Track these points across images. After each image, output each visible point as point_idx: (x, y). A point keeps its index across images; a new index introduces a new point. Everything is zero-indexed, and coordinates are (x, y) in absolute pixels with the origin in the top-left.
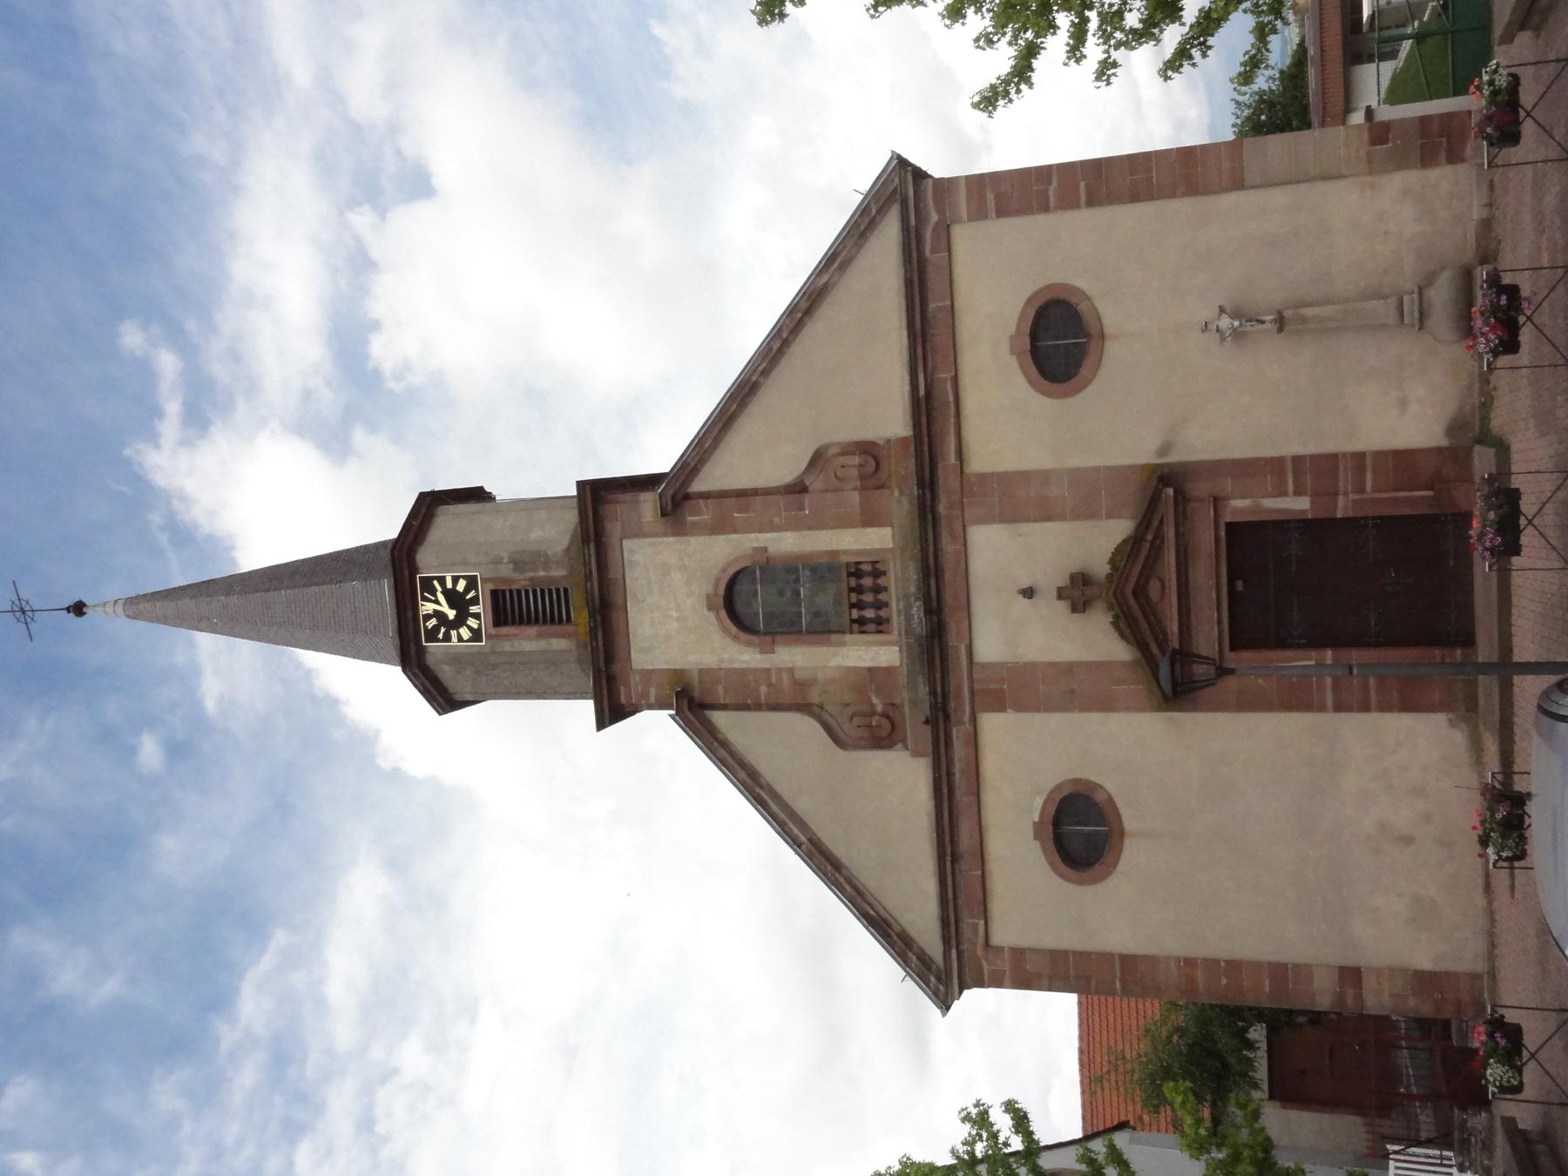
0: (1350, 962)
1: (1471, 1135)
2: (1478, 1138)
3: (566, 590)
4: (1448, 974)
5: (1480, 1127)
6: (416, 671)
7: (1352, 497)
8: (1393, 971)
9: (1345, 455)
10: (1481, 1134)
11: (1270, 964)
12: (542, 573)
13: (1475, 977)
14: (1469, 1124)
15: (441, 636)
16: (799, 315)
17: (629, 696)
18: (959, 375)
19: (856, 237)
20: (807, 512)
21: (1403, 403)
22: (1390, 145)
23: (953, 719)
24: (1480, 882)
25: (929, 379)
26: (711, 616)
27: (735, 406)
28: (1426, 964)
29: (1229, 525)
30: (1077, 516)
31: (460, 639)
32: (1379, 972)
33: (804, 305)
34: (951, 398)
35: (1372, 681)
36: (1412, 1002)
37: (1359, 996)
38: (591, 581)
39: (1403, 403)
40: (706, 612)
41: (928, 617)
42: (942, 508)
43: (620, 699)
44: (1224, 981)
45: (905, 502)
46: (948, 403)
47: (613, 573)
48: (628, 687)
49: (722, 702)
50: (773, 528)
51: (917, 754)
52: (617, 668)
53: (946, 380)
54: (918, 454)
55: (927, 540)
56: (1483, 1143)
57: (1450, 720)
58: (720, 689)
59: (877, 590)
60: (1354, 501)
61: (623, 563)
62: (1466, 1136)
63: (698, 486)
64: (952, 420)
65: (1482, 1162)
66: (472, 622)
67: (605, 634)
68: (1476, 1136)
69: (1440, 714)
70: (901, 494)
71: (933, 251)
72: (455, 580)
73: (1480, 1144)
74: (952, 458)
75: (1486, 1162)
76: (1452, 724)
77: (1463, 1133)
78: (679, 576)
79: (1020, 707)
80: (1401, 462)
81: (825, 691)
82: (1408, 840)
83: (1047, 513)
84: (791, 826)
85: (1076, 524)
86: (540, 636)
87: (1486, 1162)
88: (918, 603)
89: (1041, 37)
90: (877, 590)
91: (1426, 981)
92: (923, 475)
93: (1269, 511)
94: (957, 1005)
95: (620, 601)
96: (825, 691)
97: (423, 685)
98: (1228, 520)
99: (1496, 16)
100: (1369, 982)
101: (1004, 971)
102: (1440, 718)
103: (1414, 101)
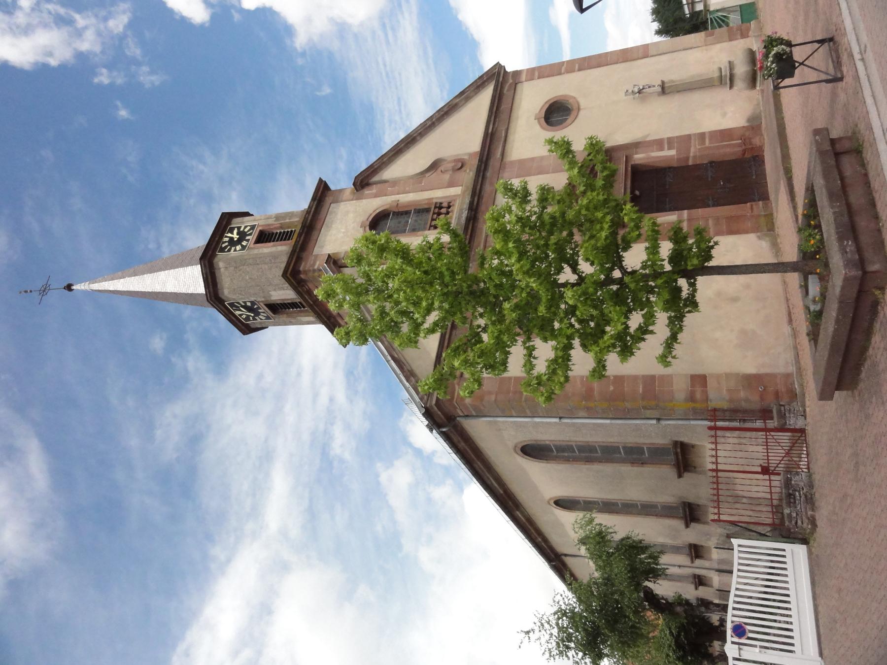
0: (700, 371)
1: (796, 490)
2: (802, 493)
4: (767, 375)
5: (802, 484)
6: (206, 262)
7: (698, 147)
8: (728, 376)
9: (695, 134)
10: (803, 489)
11: (643, 376)
12: (287, 221)
13: (788, 376)
14: (793, 482)
16: (443, 113)
17: (305, 267)
18: (509, 128)
19: (475, 87)
23: (471, 259)
24: (785, 319)
25: (494, 129)
27: (403, 145)
28: (751, 369)
31: (261, 319)
32: (718, 377)
33: (445, 109)
34: (503, 135)
36: (742, 394)
37: (705, 393)
38: (309, 215)
40: (359, 228)
41: (470, 211)
42: (488, 174)
43: (299, 267)
44: (612, 388)
46: (524, 523)
47: (322, 215)
48: (306, 264)
52: (304, 255)
54: (480, 160)
55: (478, 182)
56: (806, 496)
60: (699, 149)
61: (328, 212)
62: (791, 491)
63: (376, 178)
64: (502, 142)
65: (806, 513)
66: (244, 243)
67: (305, 238)
68: (799, 492)
69: (752, 234)
71: (508, 90)
73: (803, 497)
74: (498, 155)
75: (810, 513)
76: (759, 238)
77: (789, 490)
78: (352, 215)
80: (725, 134)
82: (735, 300)
85: (553, 175)
86: (274, 246)
87: (810, 513)
89: (646, 313)
90: (448, 213)
91: (752, 381)
92: (483, 157)
93: (653, 157)
95: (319, 227)
97: (206, 274)
100: (711, 384)
102: (752, 237)
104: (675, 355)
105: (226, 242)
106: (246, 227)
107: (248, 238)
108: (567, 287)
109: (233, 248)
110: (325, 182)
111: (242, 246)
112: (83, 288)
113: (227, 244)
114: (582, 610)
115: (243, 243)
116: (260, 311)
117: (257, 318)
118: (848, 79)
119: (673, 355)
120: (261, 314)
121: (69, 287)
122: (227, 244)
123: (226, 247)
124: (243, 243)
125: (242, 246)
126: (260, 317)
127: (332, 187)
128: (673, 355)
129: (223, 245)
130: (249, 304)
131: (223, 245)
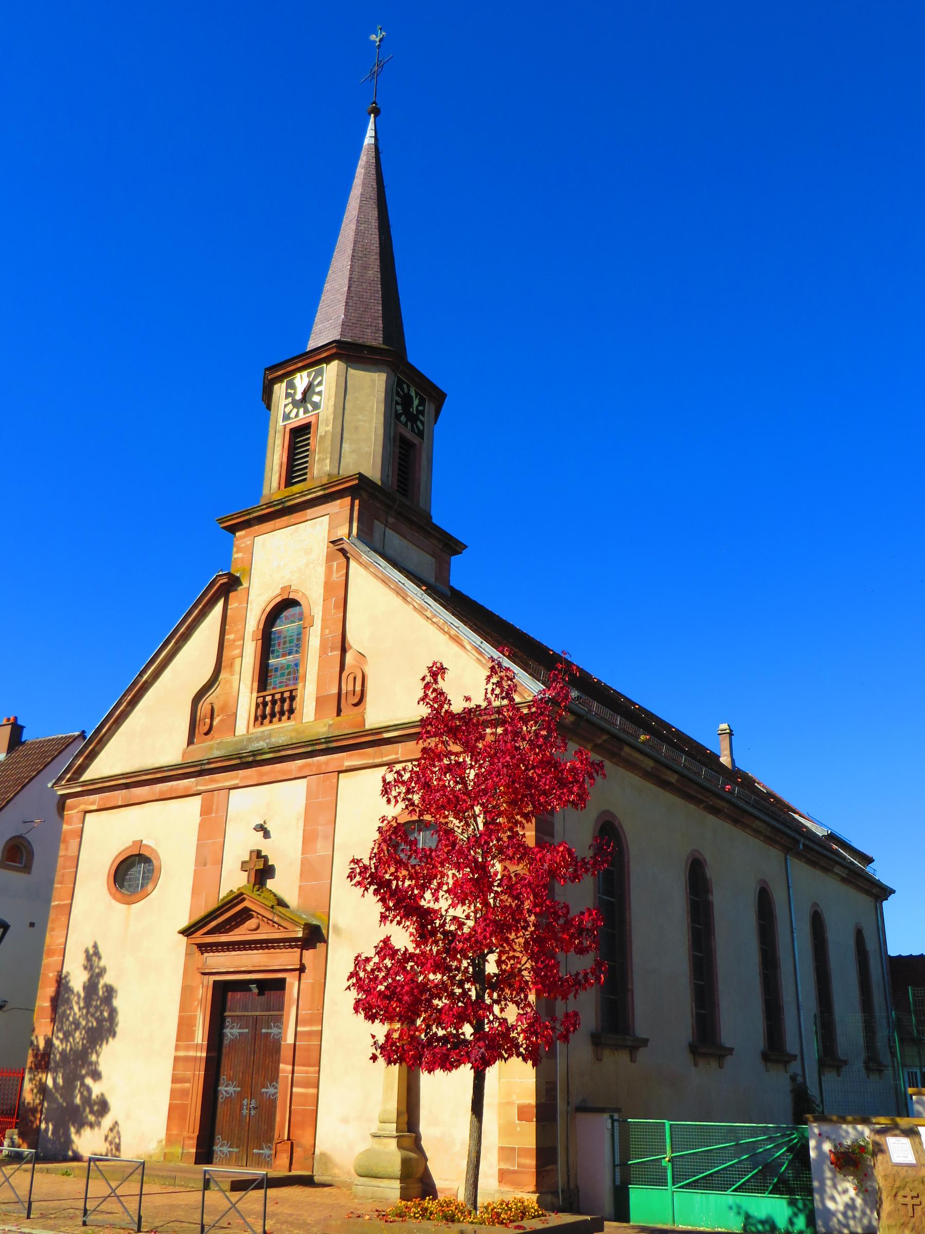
3: (305, 480)
15: (289, 391)
20: (330, 654)
21: (345, 1121)
22: (517, 1122)
26: (278, 591)
29: (283, 981)
30: (304, 862)
31: (286, 406)
35: (187, 1085)
39: (345, 1121)
45: (325, 729)
49: (229, 607)
50: (323, 629)
51: (184, 753)
53: (397, 754)
57: (161, 1141)
58: (235, 605)
59: (273, 715)
64: (371, 761)
66: (403, 419)
70: (330, 726)
72: (320, 393)
74: (348, 764)
79: (202, 825)
81: (227, 682)
83: (309, 839)
84: (173, 641)
88: (265, 745)
94: (644, 1036)
96: (227, 682)
98: (288, 980)
99: (236, 931)
101: (71, 825)
103: (233, 915)
104: (350, 990)
105: (409, 390)
106: (423, 423)
107: (409, 424)
108: (590, 779)
109: (399, 400)
110: (461, 553)
111: (401, 415)
112: (369, 128)
113: (406, 390)
114: (75, 996)
115: (403, 417)
116: (302, 410)
117: (290, 400)
118: (518, 684)
119: (352, 988)
120: (295, 410)
121: (376, 112)
122: (406, 390)
123: (403, 390)
124: (403, 417)
125: (401, 415)
126: (291, 406)
127: (454, 559)
128: (352, 988)
129: (405, 386)
130: (316, 398)
131: (405, 386)
